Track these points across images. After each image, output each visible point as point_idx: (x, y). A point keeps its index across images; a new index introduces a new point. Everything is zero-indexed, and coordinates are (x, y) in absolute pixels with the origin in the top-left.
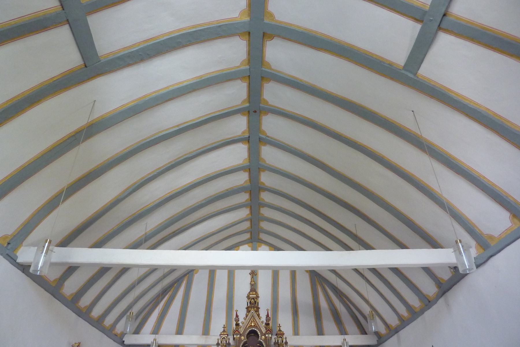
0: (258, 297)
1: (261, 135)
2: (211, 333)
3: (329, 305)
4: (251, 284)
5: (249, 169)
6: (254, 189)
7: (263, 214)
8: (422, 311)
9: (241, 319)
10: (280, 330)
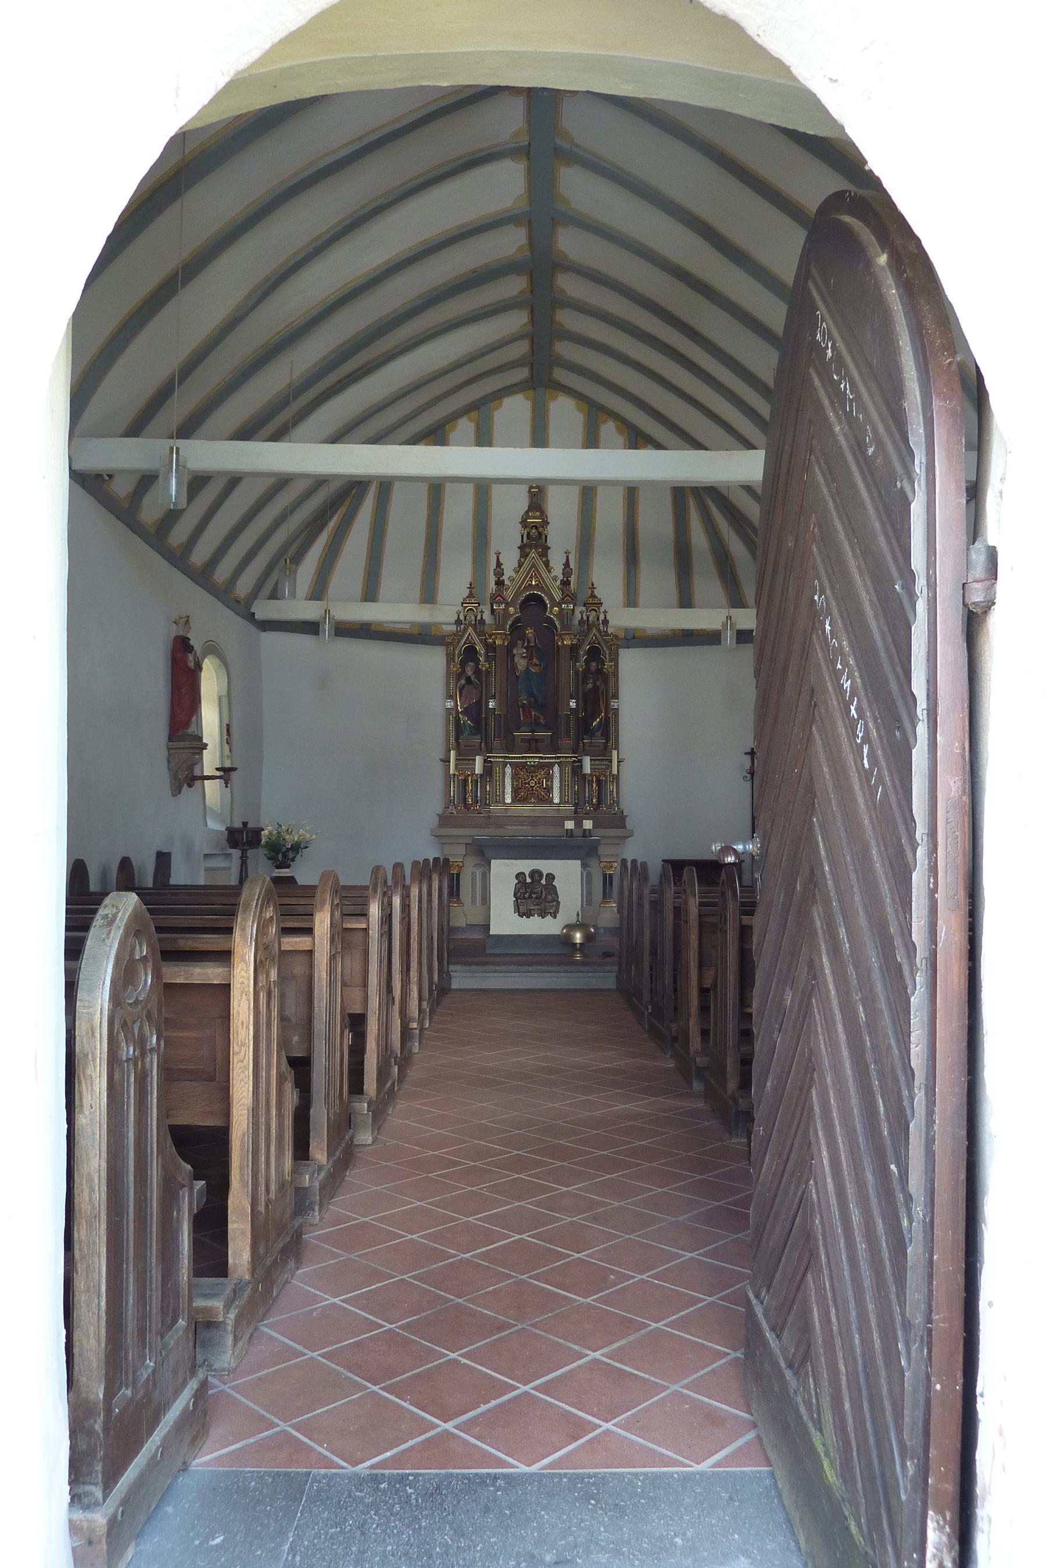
0: (545, 523)
2: (441, 597)
5: (530, 222)
6: (541, 267)
9: (508, 572)
10: (593, 596)
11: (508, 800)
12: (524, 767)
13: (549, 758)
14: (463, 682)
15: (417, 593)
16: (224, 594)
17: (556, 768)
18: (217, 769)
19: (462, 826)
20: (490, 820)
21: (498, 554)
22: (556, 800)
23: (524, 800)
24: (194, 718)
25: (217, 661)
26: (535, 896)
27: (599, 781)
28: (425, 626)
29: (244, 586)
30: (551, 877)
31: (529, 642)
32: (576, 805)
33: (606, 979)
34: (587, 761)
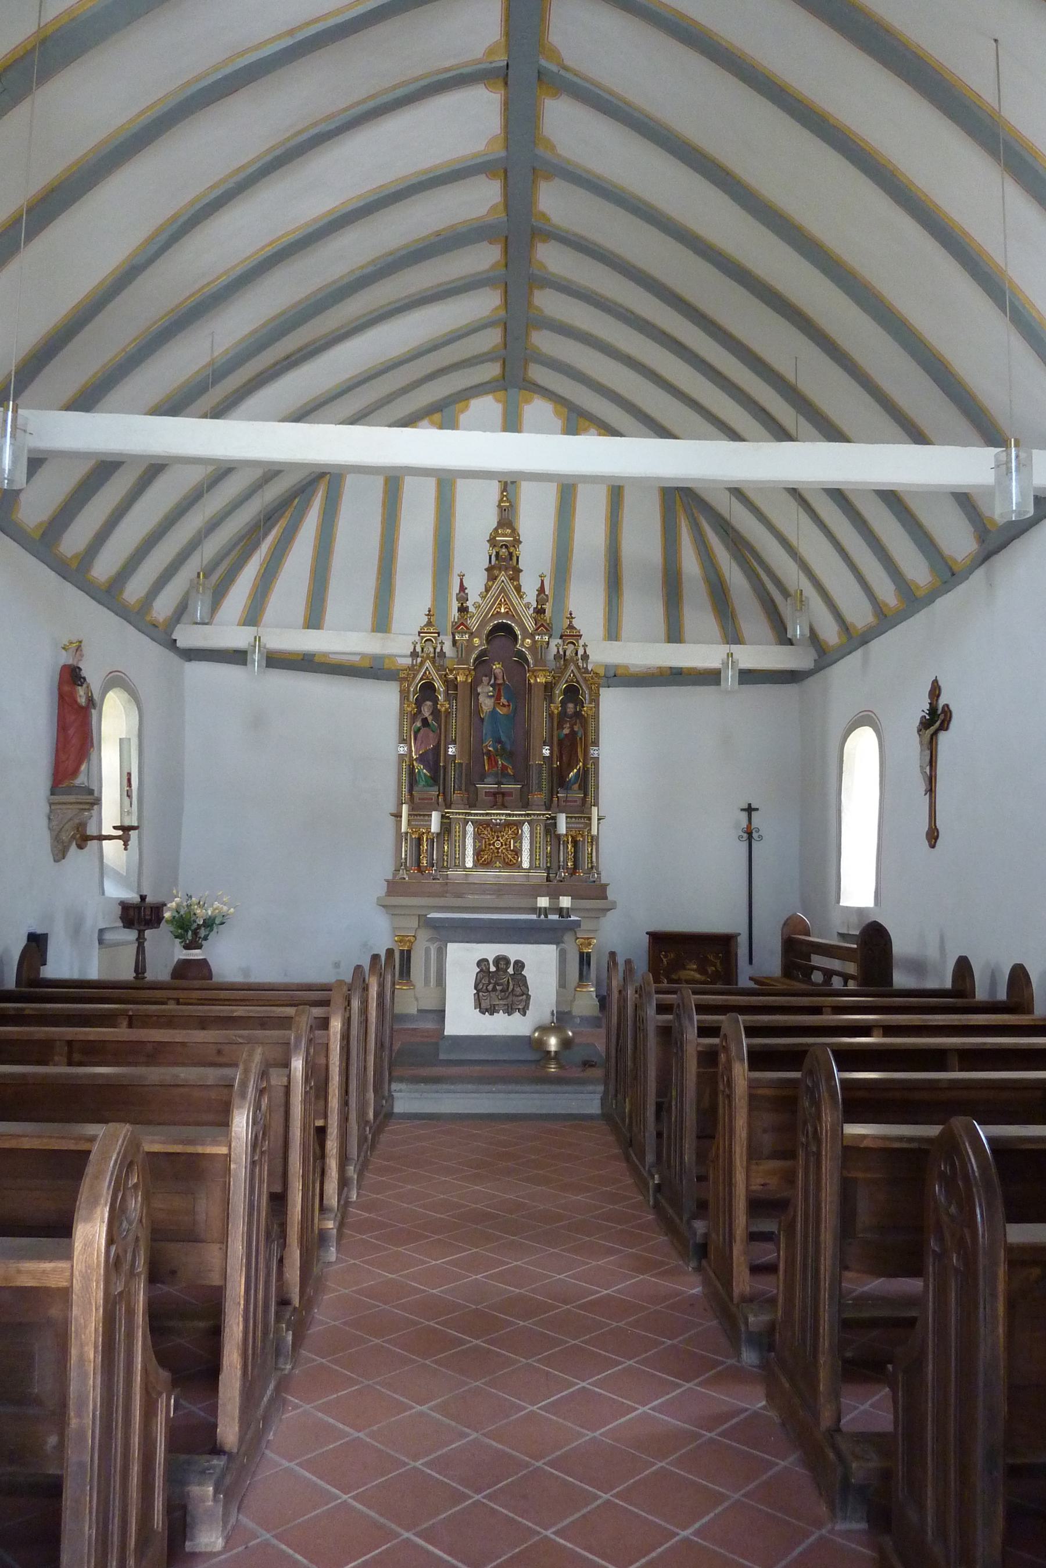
0: (517, 542)
1: (543, 63)
2: (395, 626)
3: (704, 568)
4: (499, 506)
5: (506, 171)
6: (518, 232)
7: (544, 215)
8: (931, 597)
10: (571, 627)
11: (469, 864)
12: (488, 825)
13: (517, 814)
14: (418, 724)
15: (368, 620)
16: (136, 615)
17: (526, 827)
18: (115, 828)
19: (415, 895)
20: (447, 889)
21: (462, 576)
22: (526, 865)
23: (487, 864)
24: (83, 767)
25: (126, 695)
26: (500, 987)
27: (575, 843)
28: (375, 658)
29: (163, 607)
30: (520, 965)
31: (496, 678)
32: (548, 869)
33: (589, 1101)
34: (562, 821)
